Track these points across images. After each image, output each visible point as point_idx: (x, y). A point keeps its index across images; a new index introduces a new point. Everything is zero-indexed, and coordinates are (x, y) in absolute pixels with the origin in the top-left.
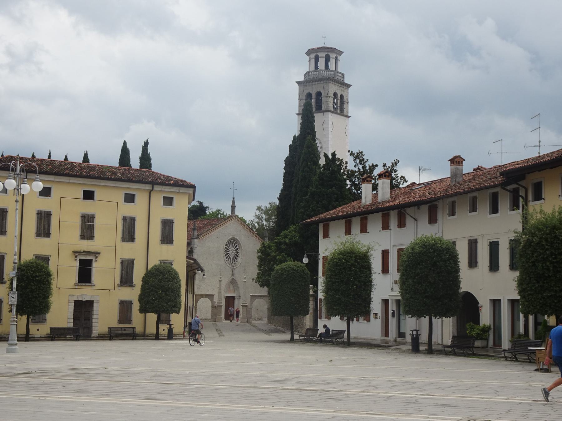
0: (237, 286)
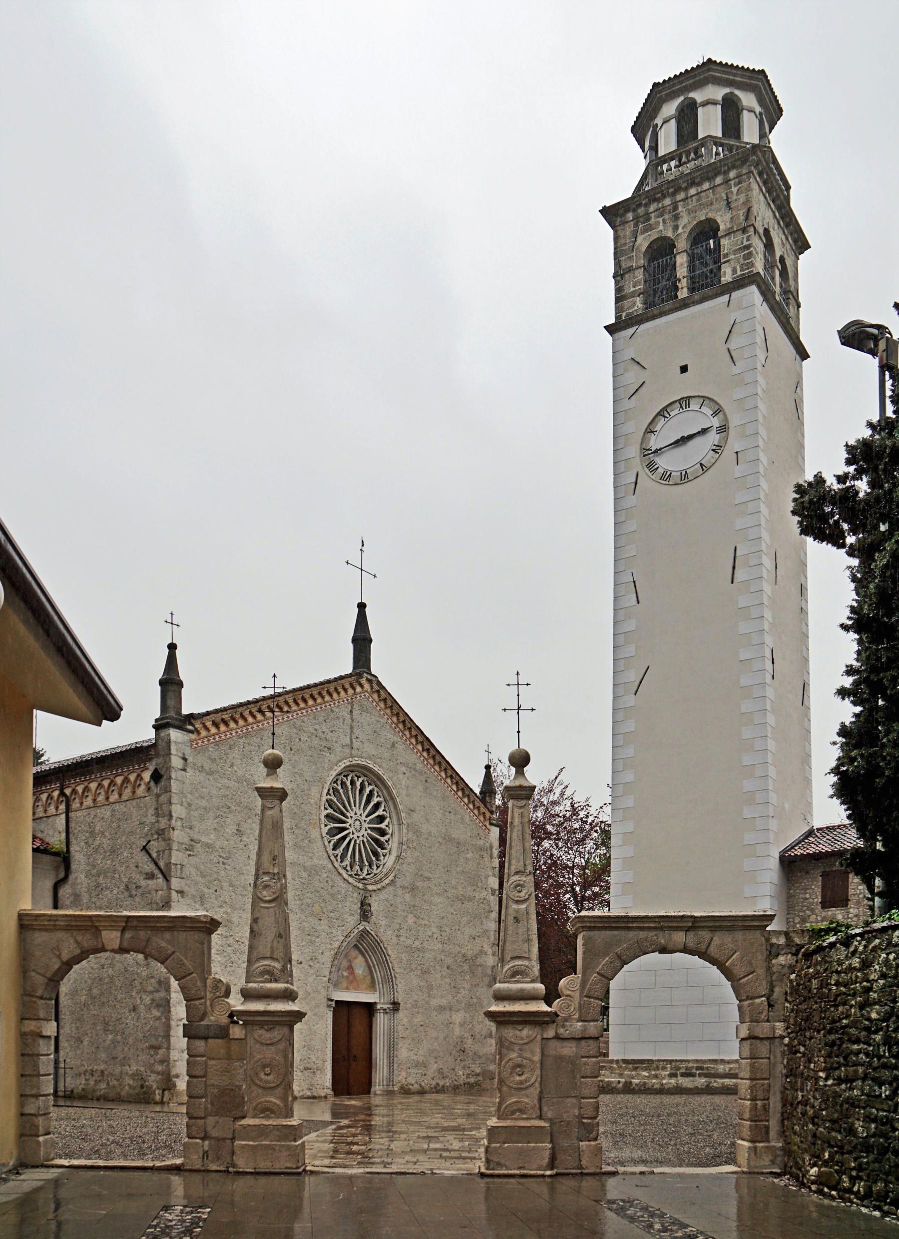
0: (385, 963)
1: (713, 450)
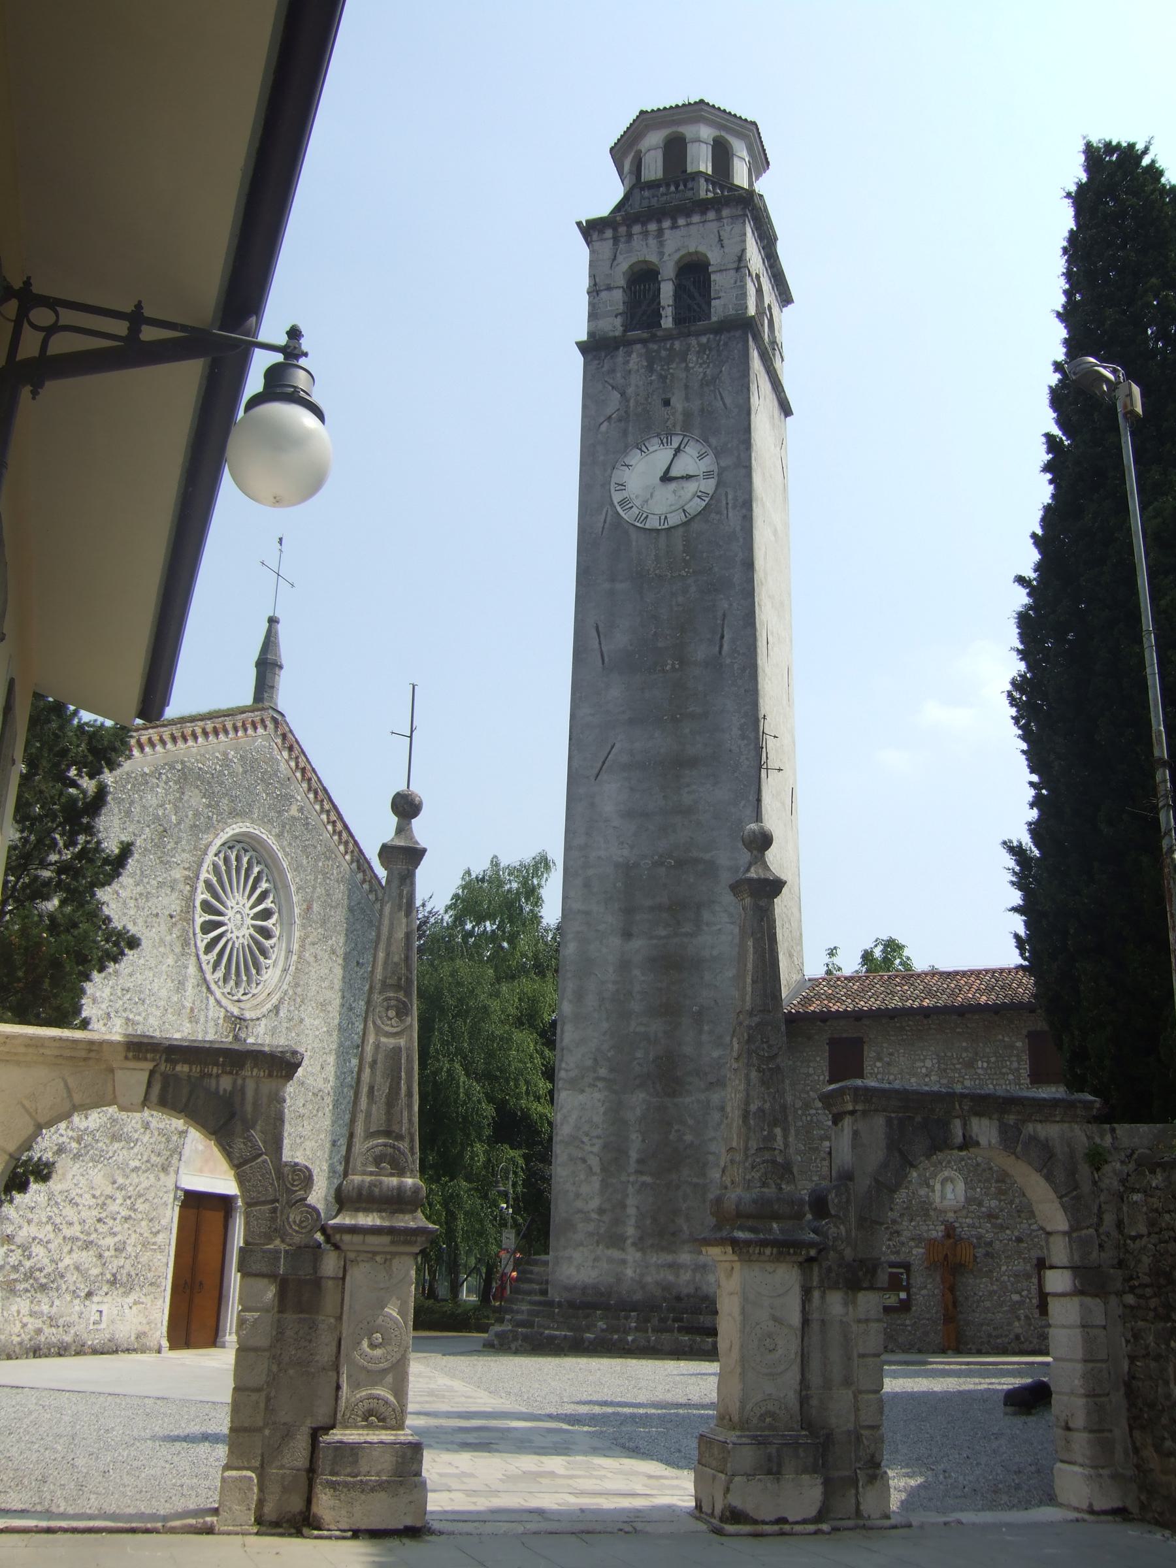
1: (698, 497)
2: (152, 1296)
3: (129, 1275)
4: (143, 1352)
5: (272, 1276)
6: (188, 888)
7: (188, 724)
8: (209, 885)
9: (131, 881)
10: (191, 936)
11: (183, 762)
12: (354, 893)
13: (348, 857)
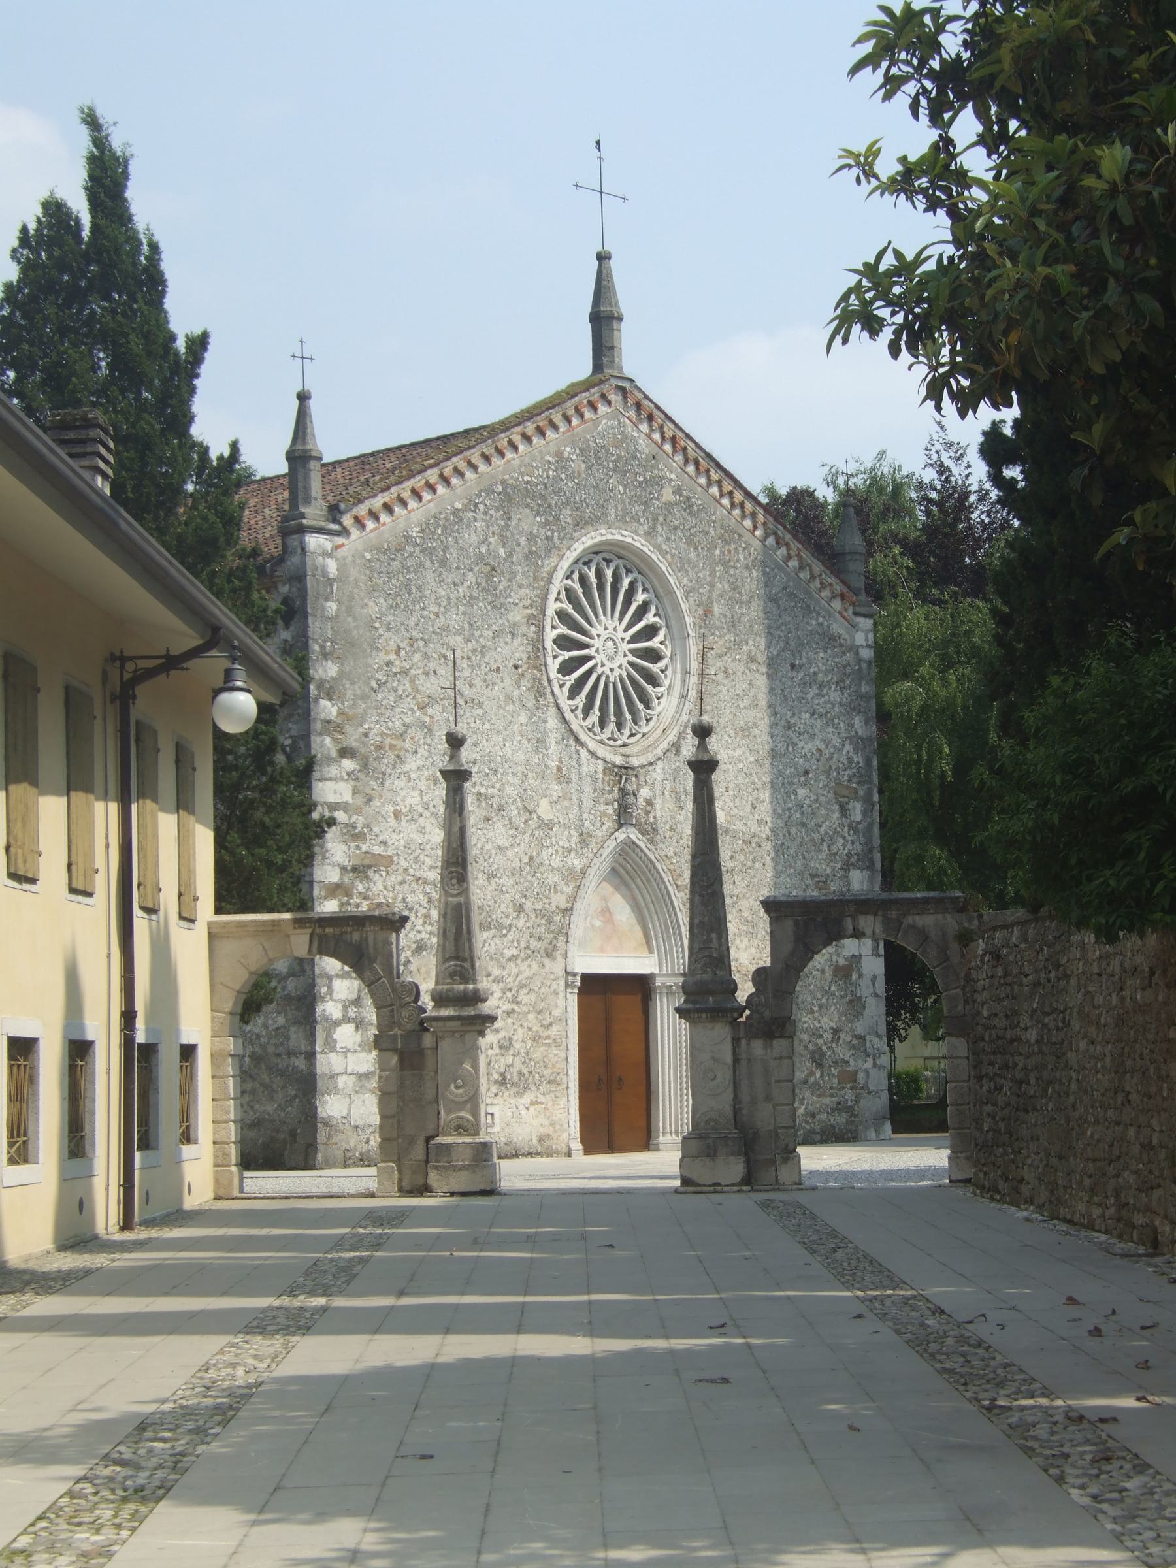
2: (552, 1095)
3: (520, 1073)
4: (549, 1155)
5: (395, 1050)
6: (533, 628)
7: (502, 435)
8: (562, 615)
9: (459, 638)
10: (546, 683)
11: (503, 482)
12: (775, 576)
13: (758, 533)
